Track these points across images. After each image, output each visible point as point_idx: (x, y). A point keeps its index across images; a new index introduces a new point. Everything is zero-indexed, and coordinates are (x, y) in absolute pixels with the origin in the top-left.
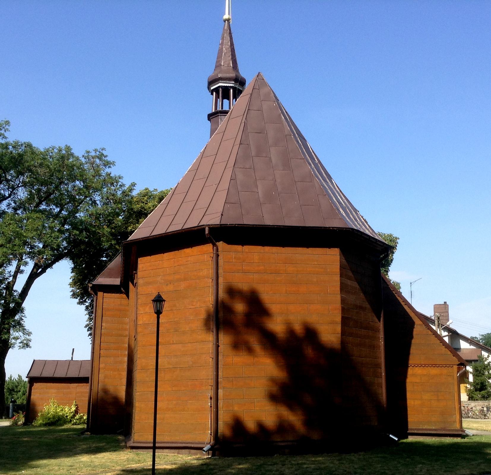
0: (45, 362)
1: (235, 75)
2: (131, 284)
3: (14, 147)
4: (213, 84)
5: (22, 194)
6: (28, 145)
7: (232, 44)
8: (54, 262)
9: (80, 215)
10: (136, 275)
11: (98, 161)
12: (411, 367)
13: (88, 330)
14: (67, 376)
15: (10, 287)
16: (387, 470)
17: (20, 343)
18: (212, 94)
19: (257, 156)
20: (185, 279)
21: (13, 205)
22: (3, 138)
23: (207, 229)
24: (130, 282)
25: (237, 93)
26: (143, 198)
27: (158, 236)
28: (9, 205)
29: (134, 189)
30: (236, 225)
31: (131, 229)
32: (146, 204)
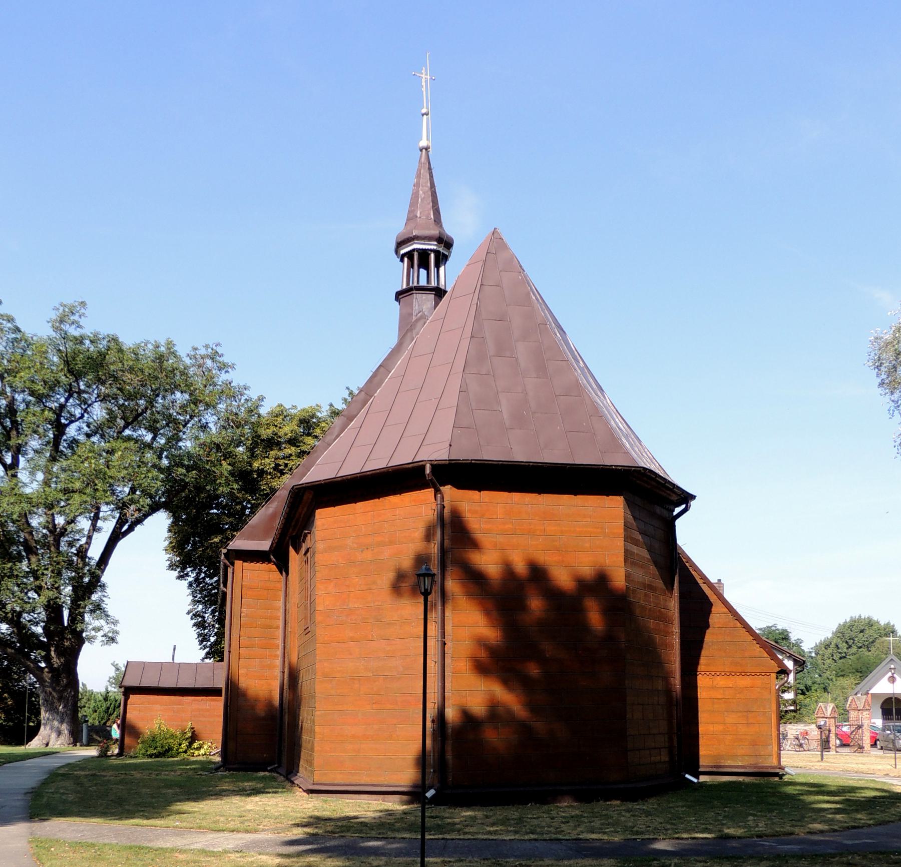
0: (144, 665)
1: (438, 232)
2: (293, 550)
3: (92, 342)
4: (404, 246)
5: (98, 412)
6: (113, 339)
7: (433, 186)
8: (146, 516)
9: (187, 444)
10: (309, 535)
11: (209, 363)
12: (700, 675)
13: (192, 619)
14: (178, 687)
15: (82, 553)
16: (446, 818)
17: (102, 636)
18: (402, 260)
19: (498, 355)
20: (392, 543)
21: (86, 429)
22: (78, 327)
23: (428, 467)
24: (291, 547)
25: (442, 259)
26: (276, 418)
27: (349, 477)
28: (80, 430)
29: (262, 406)
30: (473, 462)
31: (258, 467)
32: (280, 428)
